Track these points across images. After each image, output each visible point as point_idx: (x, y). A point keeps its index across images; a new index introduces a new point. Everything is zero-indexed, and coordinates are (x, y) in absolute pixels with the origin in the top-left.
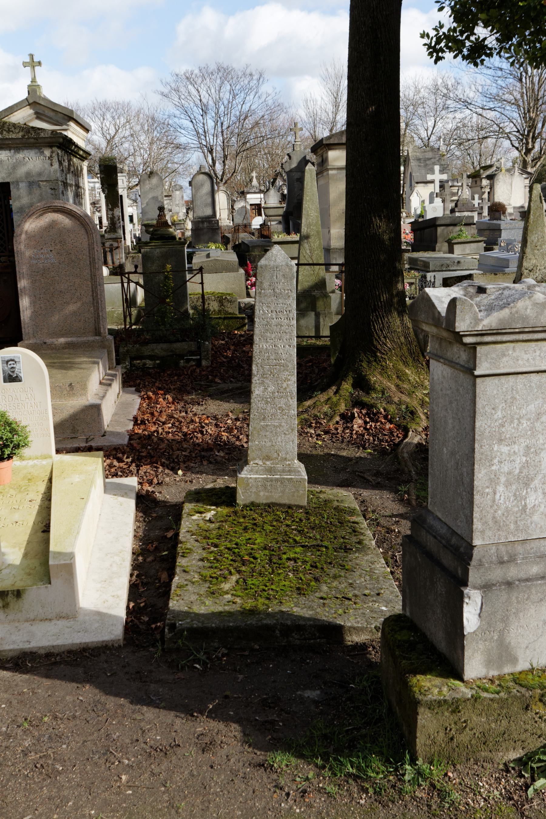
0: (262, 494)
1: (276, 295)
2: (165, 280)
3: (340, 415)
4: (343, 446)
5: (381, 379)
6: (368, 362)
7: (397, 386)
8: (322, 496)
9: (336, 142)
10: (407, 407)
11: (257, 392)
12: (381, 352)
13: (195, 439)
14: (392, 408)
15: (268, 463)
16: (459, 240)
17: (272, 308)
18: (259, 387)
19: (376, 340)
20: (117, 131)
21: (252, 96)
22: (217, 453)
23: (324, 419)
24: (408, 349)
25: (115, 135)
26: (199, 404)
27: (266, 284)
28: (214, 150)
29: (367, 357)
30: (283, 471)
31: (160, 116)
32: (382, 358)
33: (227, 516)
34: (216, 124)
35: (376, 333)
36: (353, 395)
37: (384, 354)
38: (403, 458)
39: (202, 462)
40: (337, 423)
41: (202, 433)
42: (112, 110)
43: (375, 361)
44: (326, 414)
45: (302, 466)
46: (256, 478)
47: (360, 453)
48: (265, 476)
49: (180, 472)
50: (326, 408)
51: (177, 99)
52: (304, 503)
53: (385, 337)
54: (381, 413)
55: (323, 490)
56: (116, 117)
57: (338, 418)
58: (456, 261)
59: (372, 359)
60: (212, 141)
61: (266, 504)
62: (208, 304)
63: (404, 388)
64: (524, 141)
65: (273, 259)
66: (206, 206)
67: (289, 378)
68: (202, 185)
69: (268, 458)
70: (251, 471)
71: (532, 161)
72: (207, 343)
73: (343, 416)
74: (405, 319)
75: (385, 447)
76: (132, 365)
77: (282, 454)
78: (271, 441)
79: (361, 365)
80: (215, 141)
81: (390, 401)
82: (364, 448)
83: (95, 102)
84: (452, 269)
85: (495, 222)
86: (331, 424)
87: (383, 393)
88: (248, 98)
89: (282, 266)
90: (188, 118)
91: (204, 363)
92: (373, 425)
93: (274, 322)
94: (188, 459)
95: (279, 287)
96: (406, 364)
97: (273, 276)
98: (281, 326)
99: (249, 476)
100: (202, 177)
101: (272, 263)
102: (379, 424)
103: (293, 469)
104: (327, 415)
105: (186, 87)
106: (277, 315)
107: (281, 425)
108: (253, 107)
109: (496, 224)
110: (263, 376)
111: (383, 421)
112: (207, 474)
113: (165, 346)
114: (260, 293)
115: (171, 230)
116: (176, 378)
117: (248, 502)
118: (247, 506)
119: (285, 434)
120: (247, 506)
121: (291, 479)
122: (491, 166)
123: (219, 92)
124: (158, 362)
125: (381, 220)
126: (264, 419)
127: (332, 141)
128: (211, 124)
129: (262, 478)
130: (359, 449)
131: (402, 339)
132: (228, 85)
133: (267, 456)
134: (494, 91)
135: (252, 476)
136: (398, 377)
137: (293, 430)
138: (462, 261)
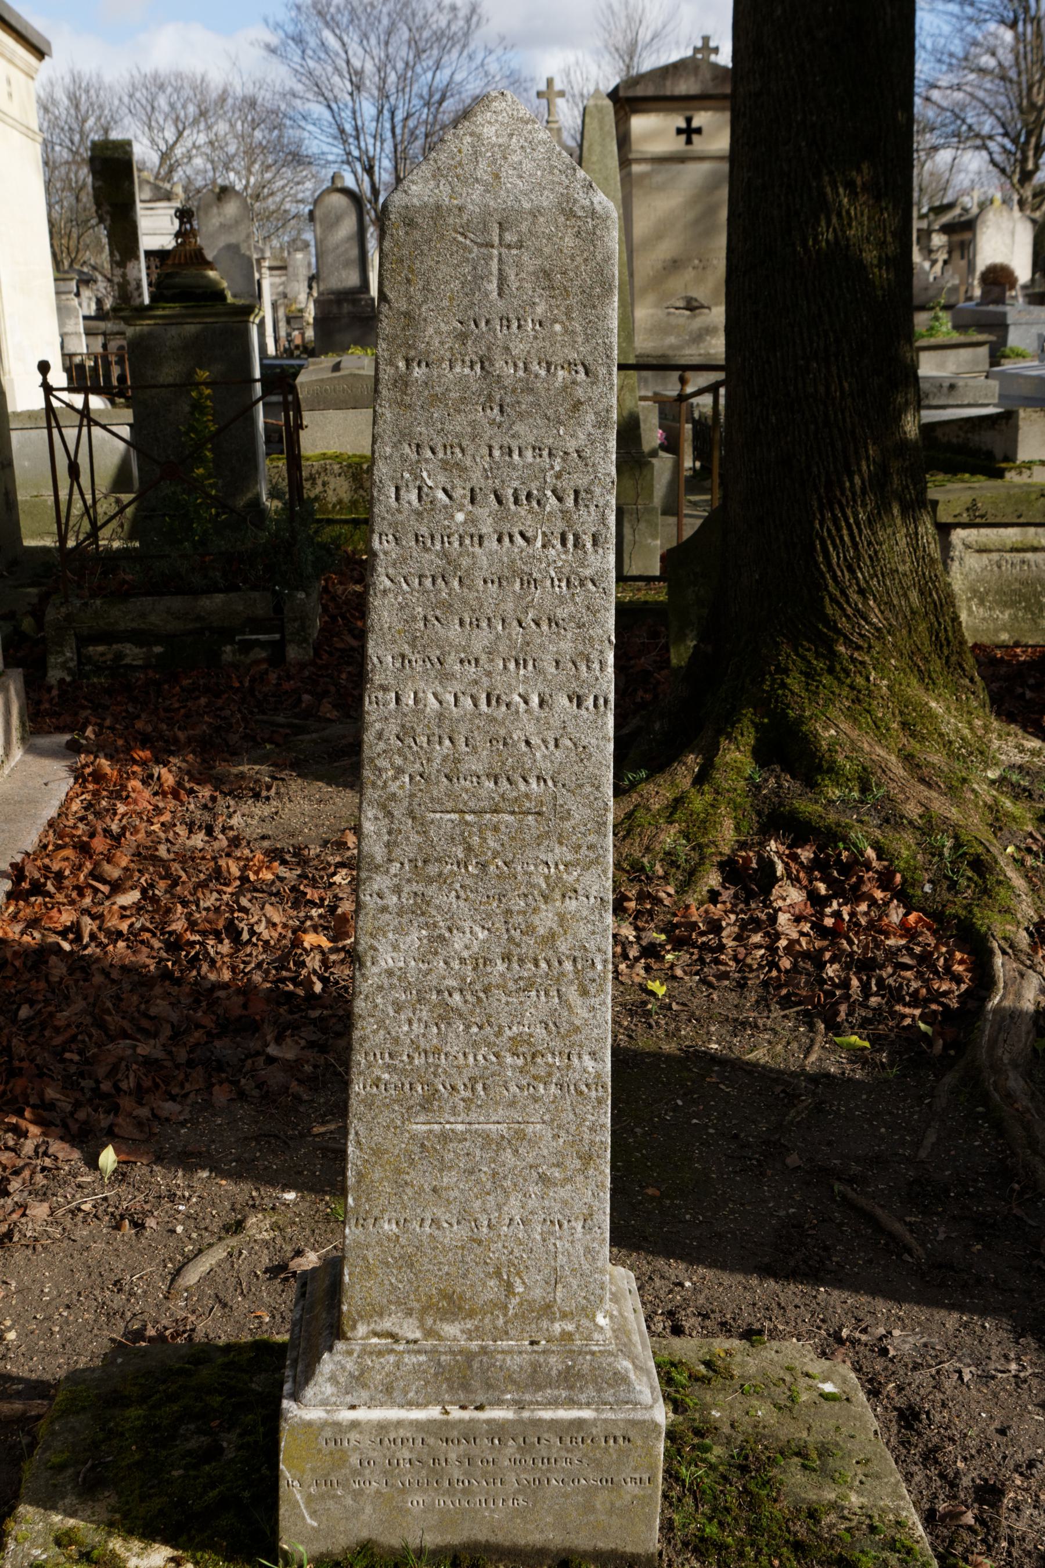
0: (416, 1501)
1: (495, 396)
2: (192, 413)
3: (721, 866)
5: (854, 734)
6: (807, 675)
7: (908, 758)
9: (650, 91)
10: (958, 845)
11: (387, 959)
12: (848, 642)
13: (205, 968)
14: (905, 846)
15: (451, 1330)
16: (933, 341)
17: (476, 478)
18: (399, 930)
19: (834, 600)
20: (180, 134)
21: (455, 53)
22: (272, 1050)
23: (665, 878)
24: (930, 630)
25: (175, 143)
26: (257, 796)
27: (437, 331)
28: (376, 169)
29: (803, 658)
30: (535, 1379)
31: (264, 97)
32: (853, 660)
34: (380, 112)
35: (835, 578)
36: (758, 788)
37: (859, 648)
38: (1009, 1096)
40: (714, 897)
41: (234, 934)
42: (169, 90)
43: (831, 671)
44: (670, 858)
46: (383, 1427)
47: (823, 1056)
48: (434, 1412)
49: (108, 1158)
50: (669, 837)
51: (297, 59)
53: (861, 592)
54: (868, 866)
56: (179, 106)
57: (713, 879)
58: (946, 384)
59: (820, 665)
60: (371, 148)
62: (324, 484)
63: (928, 764)
64: (1019, 155)
65: (483, 171)
66: (347, 264)
67: (569, 878)
68: (338, 219)
69: (452, 1305)
70: (359, 1380)
71: (1035, 196)
72: (302, 595)
73: (731, 871)
74: (921, 530)
75: (913, 1027)
76: (82, 659)
77: (531, 1287)
78: (465, 1216)
79: (784, 685)
80: (378, 149)
81: (892, 820)
82: (834, 1027)
83: (135, 73)
84: (935, 402)
85: (991, 308)
86: (691, 900)
87: (865, 789)
88: (446, 58)
89: (535, 213)
90: (321, 99)
91: (293, 653)
92: (845, 912)
93: (485, 558)
95: (519, 348)
96: (927, 679)
97: (479, 278)
98: (530, 581)
99: (346, 1415)
100: (339, 200)
101: (474, 198)
102: (863, 907)
103: (585, 1364)
104: (673, 864)
105: (316, 32)
106: (502, 516)
107: (521, 1135)
108: (458, 78)
109: (995, 313)
110: (419, 866)
111: (879, 894)
113: (177, 603)
114: (402, 382)
115: (212, 274)
116: (203, 701)
117: (339, 1542)
119: (543, 1179)
121: (580, 1423)
122: (951, 206)
123: (387, 43)
124: (158, 649)
125: (853, 195)
126: (427, 1104)
127: (640, 91)
128: (368, 109)
129: (417, 1425)
130: (812, 1027)
131: (914, 595)
132: (405, 29)
134: (957, 47)
135: (361, 1414)
136: (904, 725)
137: (587, 1159)
138: (961, 383)
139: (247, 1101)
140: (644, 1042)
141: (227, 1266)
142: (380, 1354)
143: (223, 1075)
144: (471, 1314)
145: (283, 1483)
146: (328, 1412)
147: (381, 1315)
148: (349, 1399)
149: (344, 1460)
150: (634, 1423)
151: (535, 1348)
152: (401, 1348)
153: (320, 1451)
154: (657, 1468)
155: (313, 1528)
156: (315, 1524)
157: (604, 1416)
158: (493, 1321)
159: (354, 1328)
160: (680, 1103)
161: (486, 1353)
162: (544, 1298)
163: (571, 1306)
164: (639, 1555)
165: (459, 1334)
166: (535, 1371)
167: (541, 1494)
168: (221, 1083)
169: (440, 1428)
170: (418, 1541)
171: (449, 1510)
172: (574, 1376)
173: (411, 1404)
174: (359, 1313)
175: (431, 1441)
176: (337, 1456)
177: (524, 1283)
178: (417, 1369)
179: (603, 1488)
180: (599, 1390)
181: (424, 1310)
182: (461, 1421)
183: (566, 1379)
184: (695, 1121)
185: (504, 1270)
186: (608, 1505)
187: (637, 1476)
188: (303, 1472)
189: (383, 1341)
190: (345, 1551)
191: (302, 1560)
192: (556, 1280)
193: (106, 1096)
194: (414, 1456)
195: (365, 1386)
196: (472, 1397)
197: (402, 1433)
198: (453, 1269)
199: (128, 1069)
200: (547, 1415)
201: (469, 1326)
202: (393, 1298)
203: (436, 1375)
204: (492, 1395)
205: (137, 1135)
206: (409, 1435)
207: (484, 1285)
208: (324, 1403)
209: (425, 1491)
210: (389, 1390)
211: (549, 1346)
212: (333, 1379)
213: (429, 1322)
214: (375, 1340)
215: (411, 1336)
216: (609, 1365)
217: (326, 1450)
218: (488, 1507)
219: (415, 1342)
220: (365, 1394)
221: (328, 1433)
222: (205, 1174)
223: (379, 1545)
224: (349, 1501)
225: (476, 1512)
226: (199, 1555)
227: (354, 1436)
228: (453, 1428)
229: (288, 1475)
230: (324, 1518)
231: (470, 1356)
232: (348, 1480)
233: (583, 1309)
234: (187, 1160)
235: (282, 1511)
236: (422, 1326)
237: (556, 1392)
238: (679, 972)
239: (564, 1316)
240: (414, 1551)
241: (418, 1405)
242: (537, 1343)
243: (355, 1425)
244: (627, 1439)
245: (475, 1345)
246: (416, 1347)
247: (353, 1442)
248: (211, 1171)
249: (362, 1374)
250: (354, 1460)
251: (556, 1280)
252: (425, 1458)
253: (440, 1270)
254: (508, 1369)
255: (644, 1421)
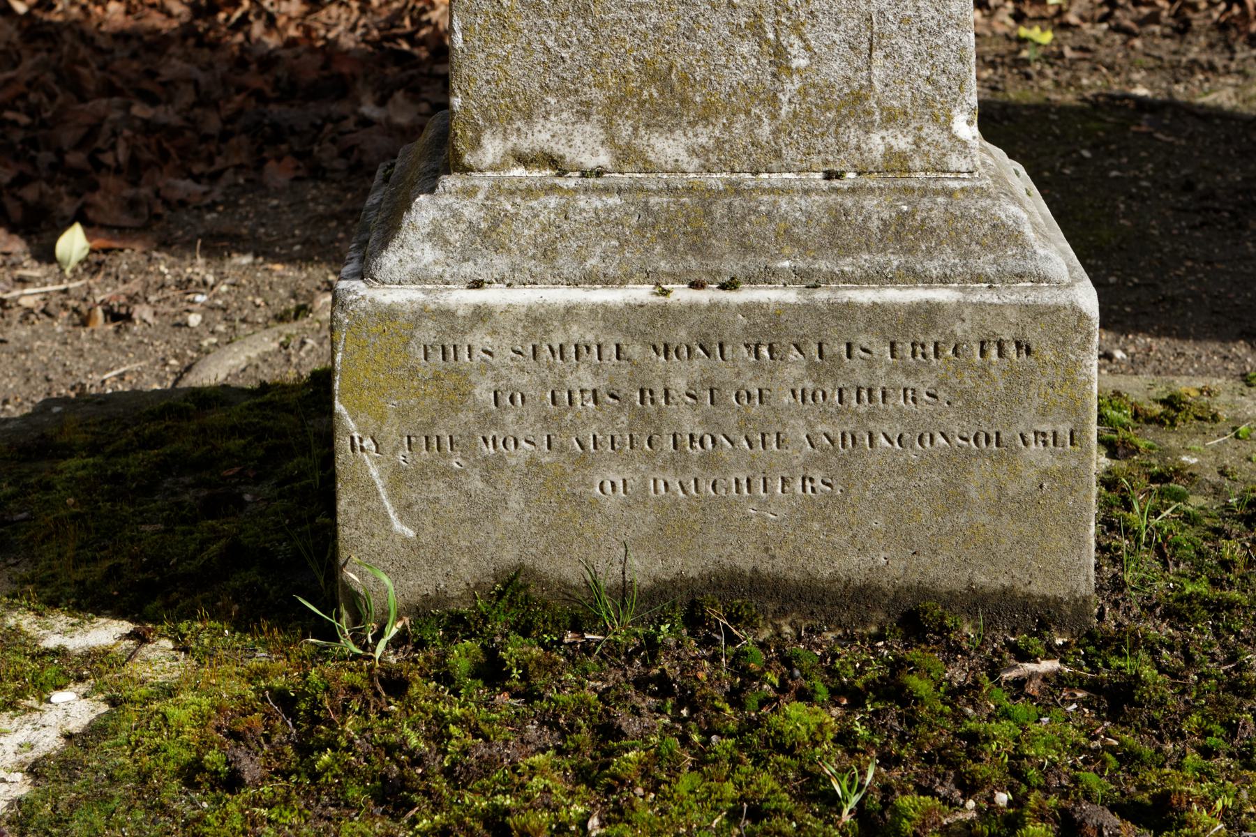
0: (610, 480)
4: (1196, 50)
8: (1194, 452)
13: (257, 29)
15: (668, 147)
22: (369, 109)
30: (838, 233)
33: (191, 774)
39: (260, 164)
45: (1018, 177)
46: (537, 319)
48: (642, 293)
49: (73, 243)
52: (1069, 566)
55: (1187, 386)
61: (655, 598)
69: (665, 95)
70: (489, 235)
94: (168, 147)
99: (462, 298)
103: (935, 210)
112: (265, 251)
117: (460, 575)
118: (457, 626)
120: (457, 626)
121: (930, 312)
129: (606, 314)
133: (660, 78)
135: (493, 296)
139: (324, 179)
140: (1016, 92)
141: (280, 360)
142: (529, 192)
143: (284, 147)
144: (706, 115)
145: (343, 443)
146: (424, 291)
147: (529, 117)
148: (468, 269)
149: (462, 392)
150: (1036, 312)
151: (836, 183)
152: (571, 183)
153: (413, 371)
154: (1086, 409)
155: (406, 540)
156: (411, 533)
157: (976, 298)
158: (750, 129)
159: (476, 144)
160: (1086, 154)
161: (738, 192)
162: (848, 80)
163: (900, 98)
164: (1058, 602)
165: (684, 157)
166: (837, 222)
167: (858, 466)
168: (279, 159)
169: (652, 322)
170: (617, 570)
171: (676, 503)
172: (913, 230)
173: (592, 279)
174: (485, 113)
175: (635, 350)
176: (448, 383)
177: (808, 48)
178: (600, 220)
179: (981, 453)
180: (965, 255)
181: (614, 106)
182: (693, 307)
183: (898, 237)
184: (1114, 173)
185: (768, 20)
186: (992, 493)
187: (1047, 428)
188: (382, 418)
189: (536, 173)
190: (472, 592)
191: (386, 613)
192: (870, 42)
193: (78, 173)
194: (602, 385)
195: (499, 248)
196: (713, 265)
197: (576, 332)
198: (668, 19)
199: (115, 134)
200: (864, 296)
201: (703, 140)
202: (552, 81)
203: (641, 228)
204: (754, 263)
205: (126, 220)
206: (590, 337)
207: (730, 51)
208: (419, 278)
209: (628, 461)
210: (548, 253)
211: (862, 180)
212: (436, 236)
213: (625, 131)
214: (519, 171)
215: (590, 163)
216: (983, 211)
217: (425, 372)
218: (752, 498)
219: (599, 173)
220: (501, 263)
221: (428, 333)
222: (246, 260)
223: (543, 582)
224: (476, 483)
225: (729, 506)
226: (183, 626)
227: (480, 339)
228: (677, 323)
229: (352, 425)
230: (428, 520)
231: (707, 197)
232: (472, 436)
233: (927, 103)
234: (218, 245)
235: (342, 505)
236: (610, 140)
237: (880, 258)
238: (1072, 18)
239: (890, 118)
240: (609, 591)
241: (607, 282)
242: (839, 176)
243: (481, 315)
244: (1023, 347)
245: (716, 180)
246: (600, 182)
247: (478, 352)
248: (256, 256)
249: (494, 226)
250: (483, 393)
251: (870, 42)
252: (624, 388)
253: (641, 20)
254: (784, 218)
255: (1058, 309)
